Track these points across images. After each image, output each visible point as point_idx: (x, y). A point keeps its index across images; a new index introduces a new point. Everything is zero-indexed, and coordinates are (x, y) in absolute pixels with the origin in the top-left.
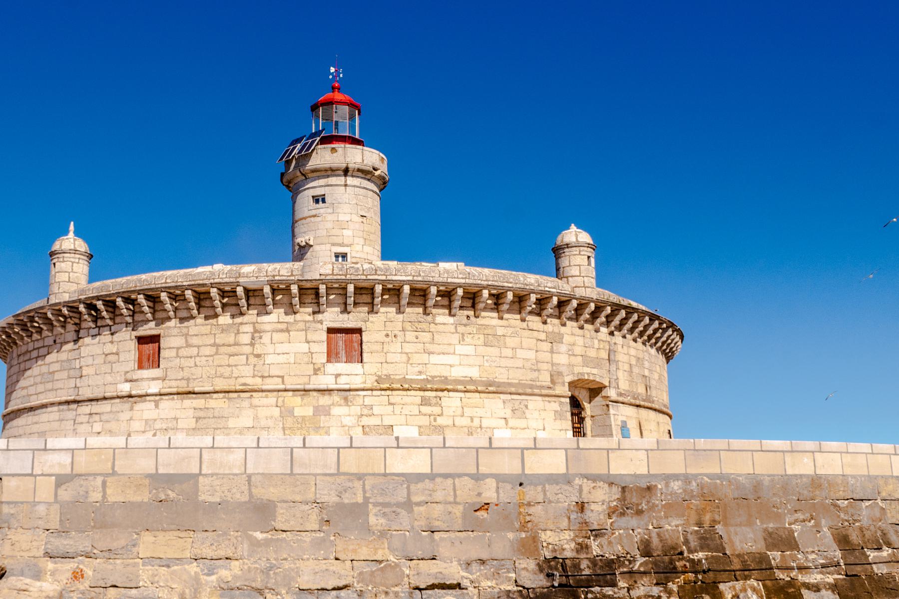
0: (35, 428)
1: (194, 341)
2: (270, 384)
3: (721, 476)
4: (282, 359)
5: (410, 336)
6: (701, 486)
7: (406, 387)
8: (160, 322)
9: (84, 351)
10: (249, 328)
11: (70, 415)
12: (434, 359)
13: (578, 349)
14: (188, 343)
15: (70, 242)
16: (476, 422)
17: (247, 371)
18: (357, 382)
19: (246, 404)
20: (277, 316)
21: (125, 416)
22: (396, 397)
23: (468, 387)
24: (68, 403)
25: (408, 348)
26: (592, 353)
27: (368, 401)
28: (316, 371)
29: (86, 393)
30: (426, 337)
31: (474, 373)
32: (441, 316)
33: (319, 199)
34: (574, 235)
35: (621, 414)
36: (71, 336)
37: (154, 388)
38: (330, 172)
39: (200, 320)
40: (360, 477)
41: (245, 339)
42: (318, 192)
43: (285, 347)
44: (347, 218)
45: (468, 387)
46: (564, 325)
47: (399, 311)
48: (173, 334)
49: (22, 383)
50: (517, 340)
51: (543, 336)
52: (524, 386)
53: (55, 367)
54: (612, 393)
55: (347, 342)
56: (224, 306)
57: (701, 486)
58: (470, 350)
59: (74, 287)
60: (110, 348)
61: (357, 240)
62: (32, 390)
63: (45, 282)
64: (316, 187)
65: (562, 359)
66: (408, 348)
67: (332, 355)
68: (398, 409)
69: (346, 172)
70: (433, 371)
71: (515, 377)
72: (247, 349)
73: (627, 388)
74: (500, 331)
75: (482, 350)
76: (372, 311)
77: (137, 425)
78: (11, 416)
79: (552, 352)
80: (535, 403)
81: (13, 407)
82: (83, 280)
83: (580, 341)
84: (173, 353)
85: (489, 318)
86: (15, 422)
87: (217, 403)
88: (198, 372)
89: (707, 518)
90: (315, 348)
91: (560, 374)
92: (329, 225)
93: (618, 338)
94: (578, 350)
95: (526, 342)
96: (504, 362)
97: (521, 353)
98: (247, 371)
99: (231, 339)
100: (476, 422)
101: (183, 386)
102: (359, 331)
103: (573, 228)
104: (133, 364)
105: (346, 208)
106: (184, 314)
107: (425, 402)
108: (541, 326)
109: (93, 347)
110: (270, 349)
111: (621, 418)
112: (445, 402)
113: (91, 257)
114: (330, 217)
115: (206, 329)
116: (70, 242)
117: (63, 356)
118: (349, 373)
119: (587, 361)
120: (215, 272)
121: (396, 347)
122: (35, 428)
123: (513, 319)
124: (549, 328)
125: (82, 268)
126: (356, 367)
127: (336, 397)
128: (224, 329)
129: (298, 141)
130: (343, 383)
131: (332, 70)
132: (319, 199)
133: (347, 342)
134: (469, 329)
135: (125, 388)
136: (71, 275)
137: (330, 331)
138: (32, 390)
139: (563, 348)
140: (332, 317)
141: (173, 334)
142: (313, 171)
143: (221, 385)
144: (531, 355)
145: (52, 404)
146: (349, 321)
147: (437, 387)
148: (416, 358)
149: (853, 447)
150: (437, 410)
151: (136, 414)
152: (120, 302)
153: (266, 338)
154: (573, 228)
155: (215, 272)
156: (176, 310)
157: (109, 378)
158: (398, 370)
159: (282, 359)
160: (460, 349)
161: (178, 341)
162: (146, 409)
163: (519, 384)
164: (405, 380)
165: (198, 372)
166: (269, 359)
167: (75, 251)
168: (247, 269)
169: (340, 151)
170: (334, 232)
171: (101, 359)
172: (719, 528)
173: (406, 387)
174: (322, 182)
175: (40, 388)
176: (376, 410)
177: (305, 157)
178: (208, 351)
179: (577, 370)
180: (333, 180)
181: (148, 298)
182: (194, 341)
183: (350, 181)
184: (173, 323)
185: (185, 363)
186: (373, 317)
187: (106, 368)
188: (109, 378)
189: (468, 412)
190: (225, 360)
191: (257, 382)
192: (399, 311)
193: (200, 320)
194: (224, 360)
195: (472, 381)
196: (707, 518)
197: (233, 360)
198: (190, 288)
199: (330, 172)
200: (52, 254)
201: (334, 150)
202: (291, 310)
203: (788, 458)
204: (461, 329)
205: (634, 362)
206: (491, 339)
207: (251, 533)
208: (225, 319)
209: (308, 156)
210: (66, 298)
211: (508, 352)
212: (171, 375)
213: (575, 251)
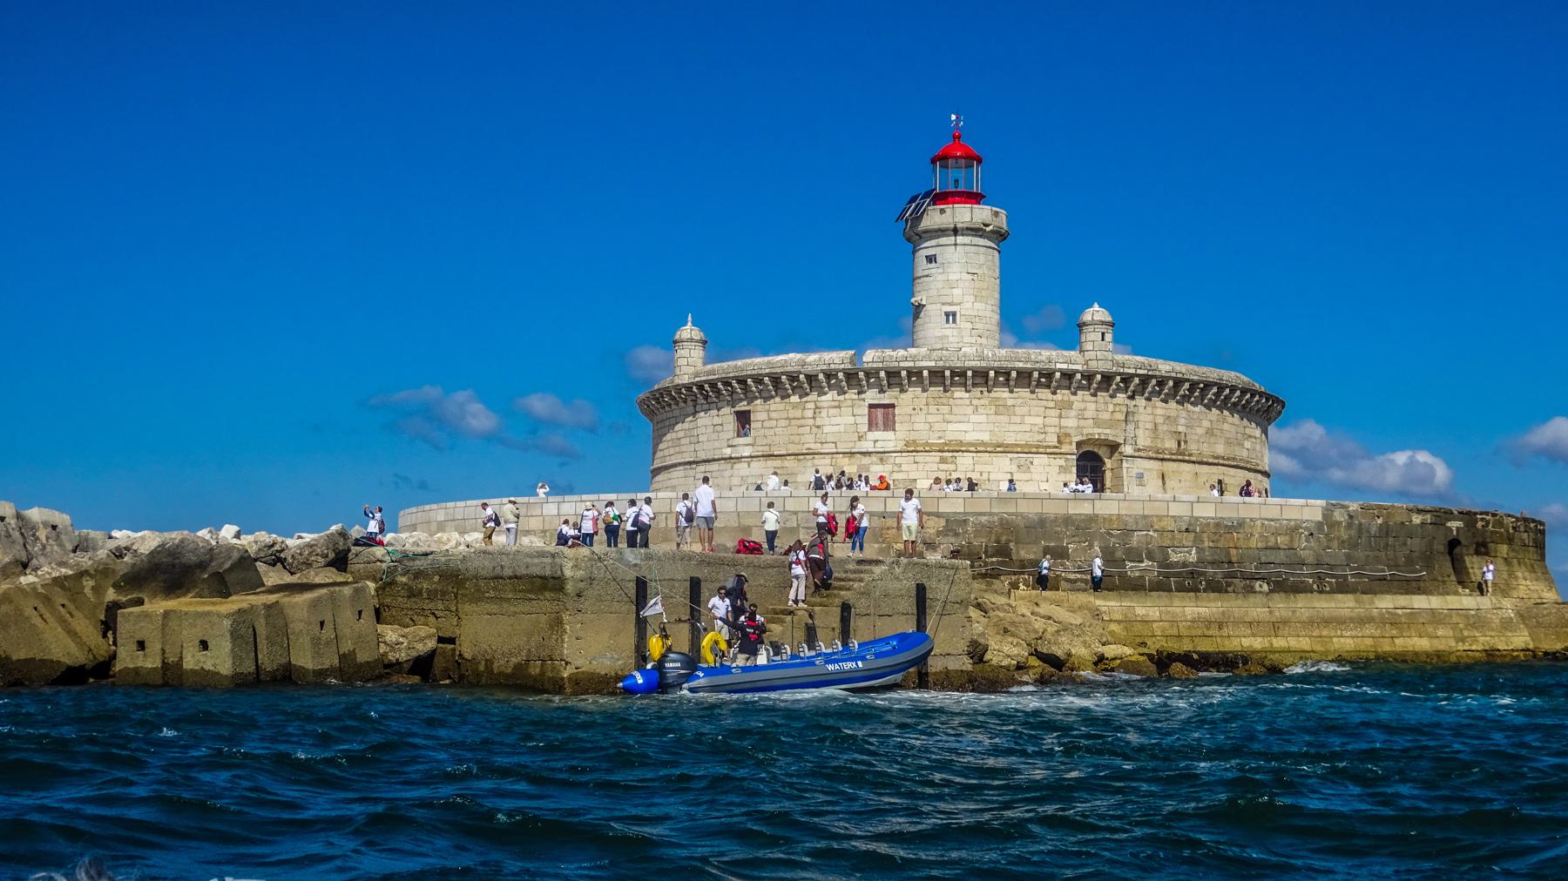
0: (669, 483)
1: (774, 415)
2: (829, 448)
3: (1016, 514)
4: (835, 429)
5: (933, 409)
6: (1001, 519)
7: (928, 449)
8: (751, 401)
9: (700, 422)
10: (811, 405)
11: (692, 473)
12: (951, 427)
13: (1089, 415)
14: (768, 413)
15: (688, 331)
16: (985, 476)
17: (810, 438)
18: (890, 446)
19: (809, 463)
20: (831, 395)
21: (727, 474)
22: (920, 457)
23: (979, 448)
24: (690, 463)
25: (931, 418)
26: (1106, 416)
27: (898, 460)
28: (860, 438)
29: (703, 456)
30: (945, 409)
31: (986, 437)
32: (959, 393)
33: (931, 259)
34: (1096, 313)
35: (1131, 468)
36: (690, 409)
37: (747, 452)
38: (941, 232)
39: (778, 399)
40: (796, 513)
41: (809, 414)
42: (930, 252)
43: (838, 420)
44: (957, 276)
45: (979, 448)
46: (1075, 394)
47: (924, 390)
48: (760, 411)
49: (661, 446)
50: (1026, 409)
51: (1052, 404)
52: (1031, 446)
53: (681, 434)
54: (1128, 450)
55: (883, 416)
56: (793, 389)
57: (1001, 519)
58: (983, 418)
59: (692, 370)
60: (717, 420)
61: (967, 298)
62: (666, 452)
63: (670, 366)
64: (928, 248)
65: (1070, 423)
66: (931, 418)
67: (872, 425)
68: (921, 466)
69: (955, 231)
70: (950, 436)
71: (1022, 439)
72: (811, 422)
73: (1148, 443)
74: (1010, 402)
75: (993, 418)
76: (902, 391)
77: (736, 481)
78: (656, 472)
79: (1060, 417)
80: (1040, 460)
81: (657, 464)
82: (699, 363)
83: (1092, 406)
84: (759, 425)
85: (1002, 393)
86: (658, 478)
87: (790, 463)
88: (777, 439)
89: (1004, 538)
90: (859, 420)
91: (1068, 435)
92: (940, 285)
93: (1140, 401)
94: (1088, 414)
95: (1034, 410)
96: (1012, 427)
97: (1028, 420)
98: (810, 438)
99: (798, 413)
100: (985, 476)
101: (766, 450)
102: (893, 406)
103: (1096, 307)
104: (731, 434)
105: (956, 268)
106: (765, 394)
107: (943, 461)
108: (1050, 396)
109: (705, 420)
110: (826, 421)
111: (1136, 471)
112: (959, 460)
113: (705, 342)
114: (940, 277)
115: (781, 407)
116: (688, 331)
117: (686, 426)
118: (886, 439)
119: (1097, 422)
120: (790, 360)
121: (921, 418)
122: (669, 483)
123: (1024, 393)
124: (1058, 397)
125: (697, 354)
126: (890, 435)
127: (874, 458)
128: (795, 406)
129: (913, 200)
130: (880, 447)
131: (953, 117)
132: (931, 259)
133: (883, 416)
134: (982, 402)
135: (728, 452)
136: (690, 364)
137: (871, 406)
138: (666, 452)
139: (1073, 413)
140: (872, 396)
141: (760, 411)
142: (926, 232)
143: (793, 449)
144: (1039, 421)
145: (680, 464)
146: (886, 399)
147: (954, 449)
148: (937, 427)
149: (469, 503)
150: (952, 467)
151: (735, 472)
152: (720, 385)
153: (824, 412)
154: (1096, 307)
155: (790, 360)
156: (760, 392)
157: (717, 444)
158: (923, 435)
159: (835, 429)
160: (974, 418)
161: (763, 416)
162: (742, 468)
163: (1026, 445)
164: (927, 444)
165: (777, 439)
166: (826, 429)
167: (691, 340)
168: (812, 358)
169: (949, 211)
170: (944, 292)
171: (710, 429)
172: (1012, 545)
173: (928, 449)
174: (933, 242)
175: (672, 451)
176: (904, 468)
177: (917, 219)
178: (783, 423)
179: (1085, 431)
180: (943, 240)
181: (739, 382)
182: (774, 415)
183: (960, 239)
184: (758, 401)
185: (768, 432)
186: (903, 396)
187: (715, 436)
188: (717, 444)
189: (978, 468)
190: (794, 430)
191: (817, 447)
192: (924, 390)
193: (778, 399)
194: (794, 430)
195: (983, 444)
196: (1004, 538)
197: (801, 430)
198: (767, 375)
199: (941, 232)
200: (675, 342)
201: (943, 211)
202: (842, 392)
203: (1071, 503)
204: (975, 402)
205: (1160, 420)
206: (1001, 409)
207: (1347, 669)
208: (795, 399)
209: (919, 219)
210: (685, 380)
211: (1014, 419)
212: (759, 441)
213: (1091, 328)
